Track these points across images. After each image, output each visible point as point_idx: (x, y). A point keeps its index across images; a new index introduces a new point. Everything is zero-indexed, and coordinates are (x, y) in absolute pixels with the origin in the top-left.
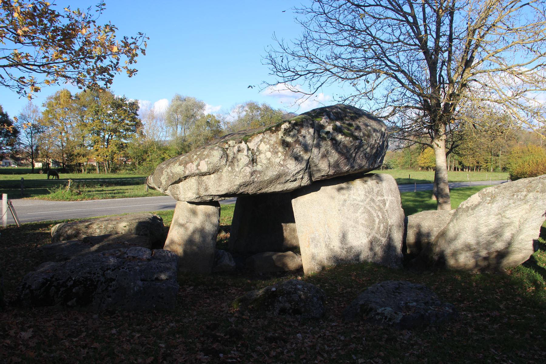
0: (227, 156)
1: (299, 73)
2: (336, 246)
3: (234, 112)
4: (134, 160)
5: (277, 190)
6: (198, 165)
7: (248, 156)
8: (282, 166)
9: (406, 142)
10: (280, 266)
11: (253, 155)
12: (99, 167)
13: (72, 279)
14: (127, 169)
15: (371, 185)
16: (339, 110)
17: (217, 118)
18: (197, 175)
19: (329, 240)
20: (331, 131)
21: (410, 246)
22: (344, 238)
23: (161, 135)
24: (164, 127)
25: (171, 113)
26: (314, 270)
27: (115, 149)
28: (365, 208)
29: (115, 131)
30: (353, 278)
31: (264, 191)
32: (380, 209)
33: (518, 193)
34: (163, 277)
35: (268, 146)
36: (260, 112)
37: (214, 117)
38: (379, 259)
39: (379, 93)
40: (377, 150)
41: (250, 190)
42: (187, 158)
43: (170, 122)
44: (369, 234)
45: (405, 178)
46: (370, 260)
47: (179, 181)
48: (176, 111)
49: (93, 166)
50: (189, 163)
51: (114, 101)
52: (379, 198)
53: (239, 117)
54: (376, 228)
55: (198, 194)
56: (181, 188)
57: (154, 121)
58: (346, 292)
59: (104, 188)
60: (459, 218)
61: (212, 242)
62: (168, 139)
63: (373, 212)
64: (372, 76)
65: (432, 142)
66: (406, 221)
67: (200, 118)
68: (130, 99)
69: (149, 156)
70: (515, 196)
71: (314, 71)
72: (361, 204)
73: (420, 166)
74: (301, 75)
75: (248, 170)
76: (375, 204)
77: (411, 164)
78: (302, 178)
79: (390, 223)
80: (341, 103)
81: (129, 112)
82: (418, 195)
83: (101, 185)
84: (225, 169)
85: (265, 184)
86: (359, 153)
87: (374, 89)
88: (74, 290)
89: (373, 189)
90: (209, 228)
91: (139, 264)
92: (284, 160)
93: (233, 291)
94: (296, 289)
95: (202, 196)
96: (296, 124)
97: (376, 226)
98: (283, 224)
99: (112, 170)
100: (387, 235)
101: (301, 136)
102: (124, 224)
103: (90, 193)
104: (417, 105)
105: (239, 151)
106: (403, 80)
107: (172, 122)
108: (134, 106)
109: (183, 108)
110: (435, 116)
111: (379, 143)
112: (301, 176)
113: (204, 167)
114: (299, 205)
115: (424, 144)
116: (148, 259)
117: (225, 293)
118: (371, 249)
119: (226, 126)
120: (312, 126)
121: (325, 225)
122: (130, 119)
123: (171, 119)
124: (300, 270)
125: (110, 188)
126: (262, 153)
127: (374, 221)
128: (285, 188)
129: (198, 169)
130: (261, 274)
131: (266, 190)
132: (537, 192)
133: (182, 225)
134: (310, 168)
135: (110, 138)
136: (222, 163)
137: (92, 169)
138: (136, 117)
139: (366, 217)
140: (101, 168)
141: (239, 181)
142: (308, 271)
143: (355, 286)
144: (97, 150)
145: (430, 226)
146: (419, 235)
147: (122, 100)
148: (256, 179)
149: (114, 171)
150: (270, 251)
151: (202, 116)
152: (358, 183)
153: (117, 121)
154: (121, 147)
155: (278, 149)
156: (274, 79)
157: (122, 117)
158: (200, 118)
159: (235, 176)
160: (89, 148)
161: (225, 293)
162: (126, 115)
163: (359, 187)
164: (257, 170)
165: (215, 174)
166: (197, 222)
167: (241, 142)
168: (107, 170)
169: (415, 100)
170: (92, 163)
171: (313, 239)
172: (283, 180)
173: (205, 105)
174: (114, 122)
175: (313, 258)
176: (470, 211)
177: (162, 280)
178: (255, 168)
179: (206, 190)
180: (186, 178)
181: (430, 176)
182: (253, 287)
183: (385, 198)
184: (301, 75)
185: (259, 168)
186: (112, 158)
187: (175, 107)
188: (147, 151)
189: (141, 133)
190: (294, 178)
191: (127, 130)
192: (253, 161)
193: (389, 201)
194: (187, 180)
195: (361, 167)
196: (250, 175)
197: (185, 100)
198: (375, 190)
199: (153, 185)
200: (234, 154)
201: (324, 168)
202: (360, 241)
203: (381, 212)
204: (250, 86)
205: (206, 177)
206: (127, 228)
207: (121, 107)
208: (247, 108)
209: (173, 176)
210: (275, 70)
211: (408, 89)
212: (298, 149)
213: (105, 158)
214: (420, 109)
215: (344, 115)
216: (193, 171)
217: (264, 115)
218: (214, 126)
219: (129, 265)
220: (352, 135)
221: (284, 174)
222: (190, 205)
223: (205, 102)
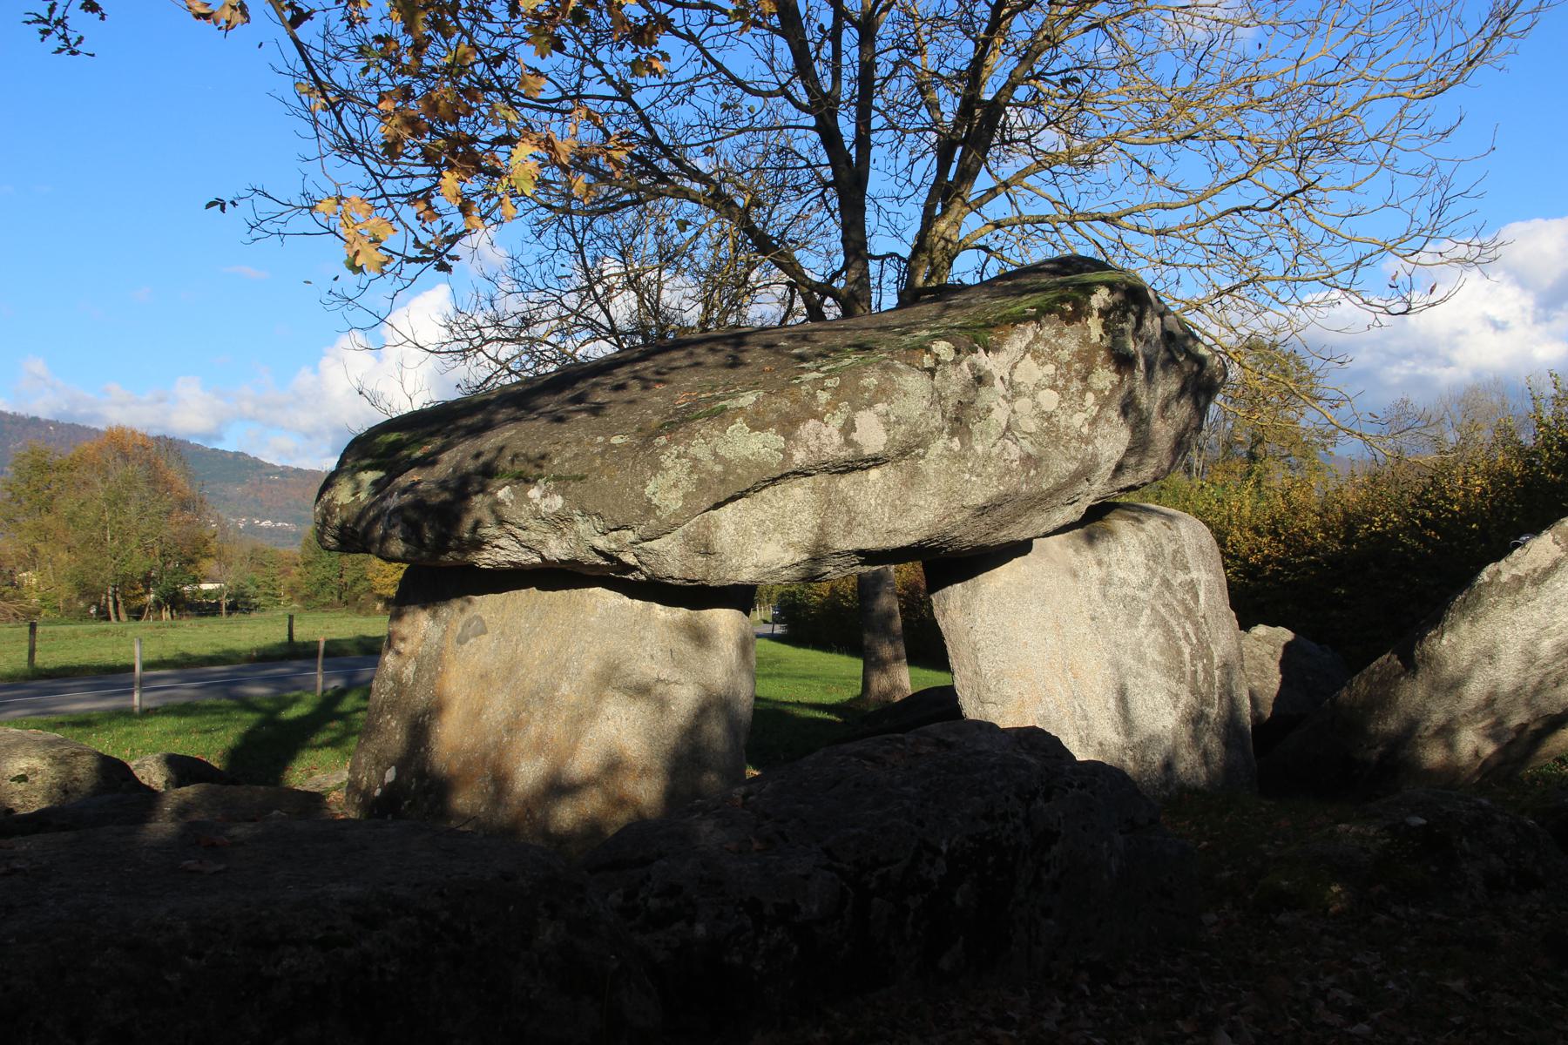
6: (848, 428)
13: (938, 852)
19: (1084, 723)
54: (1188, 674)
60: (1484, 614)
63: (1173, 622)
72: (1142, 595)
73: (380, 597)
84: (938, 446)
88: (958, 900)
97: (1188, 668)
127: (1180, 653)
129: (849, 443)
176: (1528, 590)
183: (1194, 575)
209: (726, 472)
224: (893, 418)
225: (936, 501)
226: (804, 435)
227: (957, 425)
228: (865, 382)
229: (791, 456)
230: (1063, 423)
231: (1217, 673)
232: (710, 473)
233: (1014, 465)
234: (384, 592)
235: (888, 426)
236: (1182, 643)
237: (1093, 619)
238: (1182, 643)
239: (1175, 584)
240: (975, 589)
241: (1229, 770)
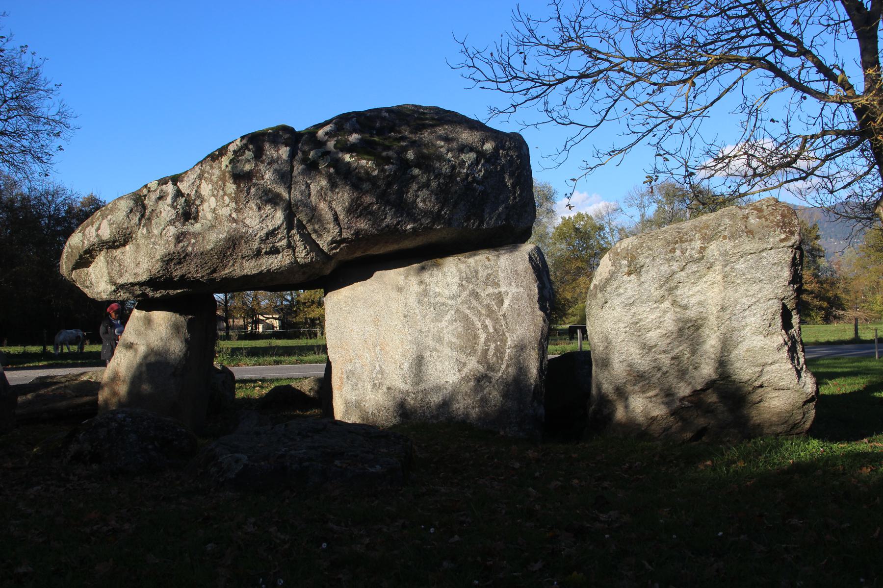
0: (144, 207)
5: (247, 272)
8: (234, 221)
19: (380, 376)
28: (457, 310)
32: (491, 313)
33: (684, 245)
52: (490, 290)
53: (643, 216)
70: (678, 252)
72: (450, 302)
75: (172, 231)
89: (477, 272)
121: (375, 346)
127: (476, 337)
132: (725, 238)
136: (133, 222)
139: (460, 329)
148: (190, 249)
159: (154, 244)
172: (244, 249)
183: (503, 289)
193: (510, 296)
198: (482, 274)
231: (508, 351)
237: (405, 317)
239: (483, 295)
241: (502, 414)
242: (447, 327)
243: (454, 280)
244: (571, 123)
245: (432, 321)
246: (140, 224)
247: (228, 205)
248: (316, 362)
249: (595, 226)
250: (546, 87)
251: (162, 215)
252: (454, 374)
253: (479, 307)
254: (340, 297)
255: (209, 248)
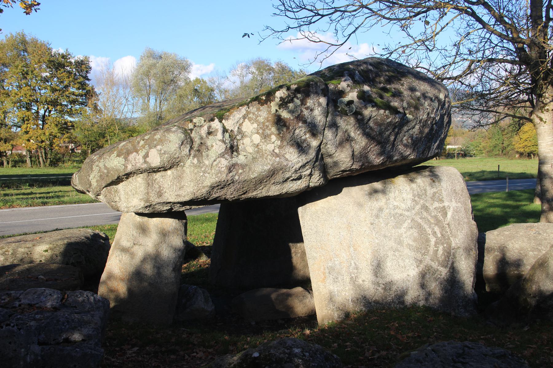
0: (192, 141)
1: (321, 12)
2: (367, 280)
3: (234, 75)
4: (84, 147)
6: (146, 156)
7: (223, 141)
8: (277, 155)
9: (491, 115)
10: (283, 310)
11: (231, 140)
12: (31, 158)
14: (74, 161)
15: (422, 184)
16: (370, 67)
17: (209, 84)
18: (145, 171)
19: (356, 271)
20: (356, 99)
21: (490, 280)
22: (378, 268)
23: (126, 109)
24: (130, 99)
25: (140, 76)
26: (333, 319)
27: (55, 130)
28: (413, 220)
29: (54, 103)
30: (392, 333)
31: (251, 195)
32: (438, 222)
34: (77, 337)
35: (255, 125)
36: (272, 74)
37: (205, 82)
38: (437, 301)
39: (446, 40)
40: (432, 129)
41: (230, 194)
42: (130, 145)
43: (139, 91)
44: (421, 261)
45: (491, 170)
46: (422, 303)
47: (118, 181)
48: (147, 74)
49: (20, 156)
50: (132, 153)
51: (51, 59)
52: (436, 205)
53: (242, 82)
54: (431, 253)
55: (147, 201)
56: (122, 192)
57: (115, 89)
58: (378, 358)
59: (35, 190)
61: (173, 275)
62: (135, 115)
63: (426, 226)
64: (434, 14)
65: (531, 113)
66: (481, 242)
67: (183, 84)
68: (77, 56)
69: (107, 141)
71: (343, 9)
72: (407, 213)
73: (517, 152)
74: (323, 16)
75: (224, 163)
76: (430, 215)
77: (504, 149)
78: (311, 175)
79: (453, 245)
80: (385, 57)
81: (75, 75)
82: (511, 196)
83: (31, 185)
84: (188, 162)
85: (251, 185)
86: (401, 135)
87: (437, 34)
89: (425, 190)
90: (166, 253)
91: (38, 317)
92: (280, 147)
93: (201, 354)
94: (292, 355)
95: (154, 203)
96: (297, 90)
97: (432, 249)
98: (291, 244)
99: (51, 161)
100: (450, 263)
101: (307, 108)
102: (44, 247)
103: (7, 198)
104: (509, 58)
105: (209, 133)
106: (486, 19)
107: (141, 90)
108: (83, 66)
109: (157, 70)
110: (537, 73)
111: (434, 118)
112: (308, 172)
113: (155, 160)
114: (309, 215)
115: (521, 118)
116: (54, 308)
117: (187, 357)
118: (423, 286)
119: (223, 96)
120: (325, 92)
121: (349, 247)
122: (77, 86)
123: (140, 85)
124: (312, 316)
125: (43, 190)
126: (246, 136)
127: (428, 240)
128: (284, 191)
129: (145, 162)
130: (253, 323)
131: (254, 193)
133: (125, 250)
134: (322, 158)
135: (47, 114)
137: (19, 161)
138: (87, 82)
139: (416, 235)
140: (33, 159)
141: (210, 180)
142: (323, 320)
143: (394, 347)
144: (27, 132)
145: (522, 249)
146: (503, 263)
147: (63, 56)
148: (237, 177)
149: (54, 163)
150: (270, 287)
151: (187, 80)
152: (400, 181)
153: (58, 88)
154: (65, 128)
155: (270, 129)
156: (281, 22)
157: (66, 83)
158: (183, 84)
159: (204, 172)
160: (14, 129)
161: (187, 357)
162: (71, 79)
163: (402, 189)
164: (239, 162)
165: (173, 170)
166: (149, 244)
167: (212, 120)
168: (44, 162)
169: (508, 50)
170: (20, 152)
171: (331, 270)
172: (279, 177)
173: (189, 65)
174: (54, 90)
175: (331, 299)
177: (75, 342)
178: (234, 160)
179: (160, 194)
180: (128, 175)
181: (530, 167)
182: (231, 348)
183: (446, 204)
184: (323, 16)
185: (241, 159)
186: (51, 144)
187: (145, 68)
188: (105, 133)
189: (95, 107)
190: (298, 175)
191: (73, 102)
192: (233, 149)
193: (451, 209)
194: (130, 179)
195: (404, 158)
196: (226, 171)
197: (161, 57)
199: (79, 187)
200: (202, 138)
201: (343, 159)
202: (404, 273)
203: (439, 227)
204: (245, 35)
205: (159, 175)
206: (49, 253)
207: (64, 68)
208: (254, 70)
209: (108, 172)
210: (283, 8)
211: (493, 32)
212: (301, 132)
213: (40, 144)
214: (513, 62)
215: (380, 74)
216: (138, 165)
217: (280, 79)
218: (205, 96)
219: (18, 319)
220: (387, 107)
221: (281, 169)
222: (138, 218)
223: (190, 61)
224: (162, 152)
225: (192, 184)
226: (130, 159)
227: (197, 153)
228: (155, 137)
229: (127, 167)
230: (264, 149)
232: (103, 173)
233: (223, 169)
234: (519, 150)
235: (161, 155)
236: (431, 236)
237: (372, 224)
238: (431, 236)
239: (431, 208)
240: (306, 209)
242: (405, 232)
243: (409, 196)
244: (320, 41)
245: (393, 227)
246: (190, 155)
247: (273, 143)
248: (75, 203)
249: (208, 88)
250: (320, 17)
251: (214, 148)
252: (414, 269)
253: (429, 217)
254: (317, 208)
255: (252, 176)
